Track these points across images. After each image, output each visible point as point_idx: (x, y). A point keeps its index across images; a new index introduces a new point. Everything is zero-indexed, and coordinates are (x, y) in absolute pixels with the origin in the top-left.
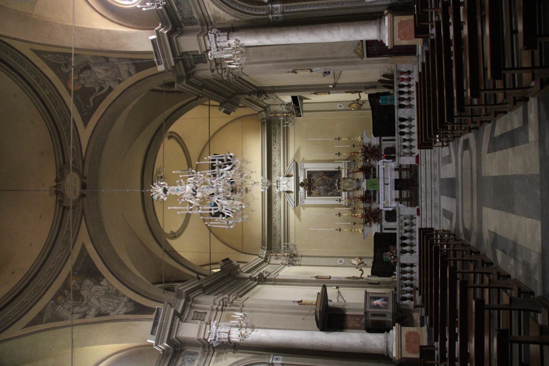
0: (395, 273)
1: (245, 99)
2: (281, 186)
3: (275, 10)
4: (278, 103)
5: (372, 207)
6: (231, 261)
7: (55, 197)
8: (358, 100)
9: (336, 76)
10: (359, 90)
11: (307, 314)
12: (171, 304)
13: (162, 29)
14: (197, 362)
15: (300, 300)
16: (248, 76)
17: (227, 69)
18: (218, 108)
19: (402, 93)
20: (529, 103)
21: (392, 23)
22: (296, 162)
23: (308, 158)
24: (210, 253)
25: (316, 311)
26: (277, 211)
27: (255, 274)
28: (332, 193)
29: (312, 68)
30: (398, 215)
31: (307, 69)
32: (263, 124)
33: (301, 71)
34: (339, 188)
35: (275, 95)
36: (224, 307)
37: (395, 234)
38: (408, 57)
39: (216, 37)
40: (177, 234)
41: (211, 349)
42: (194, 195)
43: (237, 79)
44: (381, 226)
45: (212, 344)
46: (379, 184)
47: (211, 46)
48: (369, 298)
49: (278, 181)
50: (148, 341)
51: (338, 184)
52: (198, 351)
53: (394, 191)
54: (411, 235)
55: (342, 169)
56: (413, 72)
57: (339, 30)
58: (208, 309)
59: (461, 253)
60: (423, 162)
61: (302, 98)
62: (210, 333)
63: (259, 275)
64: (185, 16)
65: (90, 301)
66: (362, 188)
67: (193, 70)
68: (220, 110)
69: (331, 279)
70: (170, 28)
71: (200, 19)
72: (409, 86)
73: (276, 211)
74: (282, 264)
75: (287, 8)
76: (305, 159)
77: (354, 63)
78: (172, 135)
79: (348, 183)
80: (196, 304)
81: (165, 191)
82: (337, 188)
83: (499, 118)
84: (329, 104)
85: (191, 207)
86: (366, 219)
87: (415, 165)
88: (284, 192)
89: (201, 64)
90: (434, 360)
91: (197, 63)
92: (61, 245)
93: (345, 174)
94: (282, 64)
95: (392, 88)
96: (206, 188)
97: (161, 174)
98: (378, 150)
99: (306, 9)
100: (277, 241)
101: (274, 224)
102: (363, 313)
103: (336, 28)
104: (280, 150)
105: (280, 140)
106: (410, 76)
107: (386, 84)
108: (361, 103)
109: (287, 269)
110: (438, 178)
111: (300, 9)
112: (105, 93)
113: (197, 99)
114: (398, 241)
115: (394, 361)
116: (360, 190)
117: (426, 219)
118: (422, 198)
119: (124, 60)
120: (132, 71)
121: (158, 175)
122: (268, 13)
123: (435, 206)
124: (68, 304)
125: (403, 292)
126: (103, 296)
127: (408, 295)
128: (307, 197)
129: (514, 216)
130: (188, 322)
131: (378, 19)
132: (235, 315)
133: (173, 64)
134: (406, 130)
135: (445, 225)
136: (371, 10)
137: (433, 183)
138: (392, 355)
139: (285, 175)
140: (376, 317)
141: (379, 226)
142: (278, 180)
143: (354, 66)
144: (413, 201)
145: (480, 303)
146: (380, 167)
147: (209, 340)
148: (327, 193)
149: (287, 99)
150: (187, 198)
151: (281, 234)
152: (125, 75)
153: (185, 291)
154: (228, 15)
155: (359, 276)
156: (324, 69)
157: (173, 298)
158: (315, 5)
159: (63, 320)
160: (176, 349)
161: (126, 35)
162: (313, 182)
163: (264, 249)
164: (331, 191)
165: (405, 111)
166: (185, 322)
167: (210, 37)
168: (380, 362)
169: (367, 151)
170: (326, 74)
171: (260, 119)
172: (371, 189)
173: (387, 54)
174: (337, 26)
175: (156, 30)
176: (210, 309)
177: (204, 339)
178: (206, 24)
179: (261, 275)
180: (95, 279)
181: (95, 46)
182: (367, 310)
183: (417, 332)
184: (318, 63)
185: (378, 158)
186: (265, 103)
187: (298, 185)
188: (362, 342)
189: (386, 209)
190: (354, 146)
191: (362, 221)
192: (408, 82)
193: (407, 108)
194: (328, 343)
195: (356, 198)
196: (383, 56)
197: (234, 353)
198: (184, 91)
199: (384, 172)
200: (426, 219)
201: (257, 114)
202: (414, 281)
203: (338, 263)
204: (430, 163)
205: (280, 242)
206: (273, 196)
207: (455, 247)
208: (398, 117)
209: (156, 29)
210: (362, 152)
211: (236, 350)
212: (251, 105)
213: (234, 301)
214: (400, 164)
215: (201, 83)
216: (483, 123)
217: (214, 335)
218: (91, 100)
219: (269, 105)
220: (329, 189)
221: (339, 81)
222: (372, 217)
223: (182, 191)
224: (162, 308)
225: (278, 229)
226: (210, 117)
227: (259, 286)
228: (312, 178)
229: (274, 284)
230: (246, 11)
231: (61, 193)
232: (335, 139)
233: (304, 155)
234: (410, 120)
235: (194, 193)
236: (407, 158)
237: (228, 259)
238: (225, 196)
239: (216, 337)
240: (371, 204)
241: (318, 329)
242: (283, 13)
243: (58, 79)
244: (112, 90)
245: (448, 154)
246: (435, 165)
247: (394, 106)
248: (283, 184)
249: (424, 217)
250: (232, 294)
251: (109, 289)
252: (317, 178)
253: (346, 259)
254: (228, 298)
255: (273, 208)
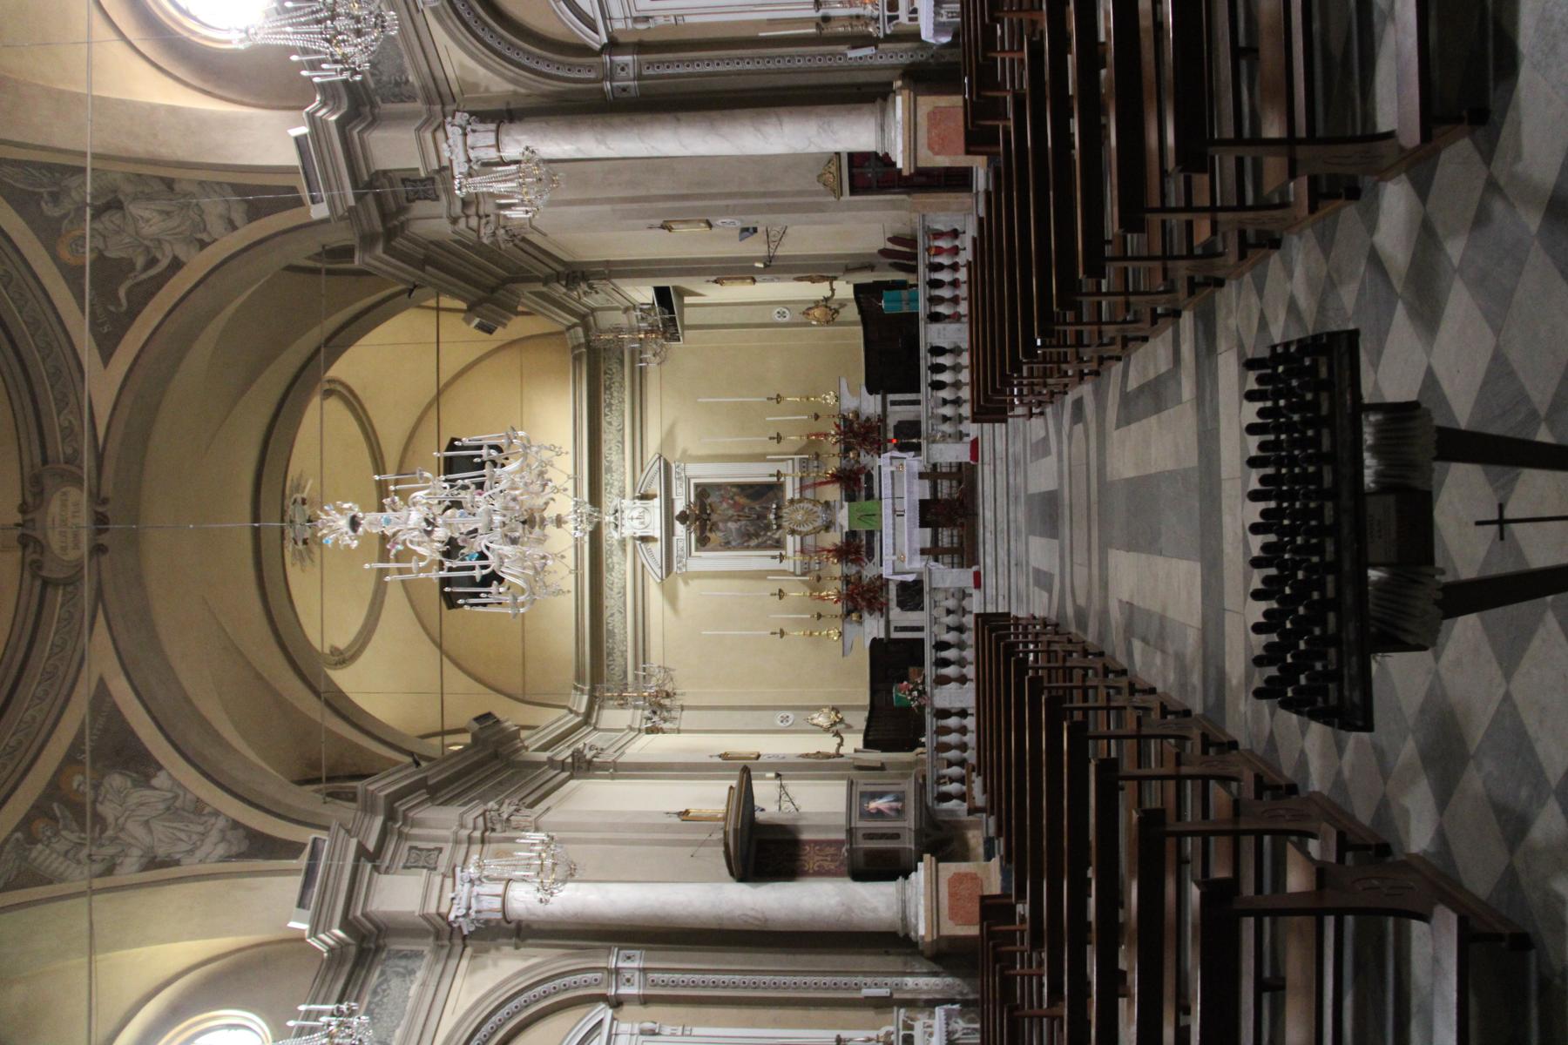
0: (923, 740)
1: (531, 293)
2: (627, 523)
3: (619, 69)
4: (617, 304)
5: (865, 573)
6: (498, 722)
7: (19, 554)
8: (826, 299)
9: (772, 239)
10: (830, 275)
11: (703, 844)
12: (348, 831)
13: (324, 111)
14: (420, 975)
15: (683, 810)
16: (545, 235)
17: (492, 218)
18: (462, 315)
19: (936, 284)
20: (1181, 320)
21: (912, 112)
22: (665, 460)
23: (695, 450)
24: (442, 694)
25: (725, 833)
26: (616, 590)
27: (564, 753)
28: (760, 540)
29: (711, 220)
30: (926, 588)
31: (700, 221)
32: (577, 359)
33: (684, 226)
34: (779, 527)
35: (613, 284)
36: (487, 834)
37: (921, 641)
38: (953, 195)
39: (465, 135)
40: (347, 655)
41: (458, 942)
42: (429, 533)
43: (517, 242)
44: (888, 623)
45: (460, 927)
46: (881, 515)
47: (453, 157)
48: (857, 798)
49: (616, 511)
50: (293, 924)
51: (776, 514)
52: (420, 948)
53: (917, 531)
54: (960, 638)
55: (785, 475)
56: (964, 232)
57: (781, 125)
58: (446, 840)
59: (1081, 672)
60: (987, 457)
61: (682, 293)
62: (453, 899)
63: (572, 755)
64: (385, 78)
65: (122, 829)
66: (837, 525)
67: (402, 218)
68: (468, 322)
69: (760, 760)
70: (344, 108)
71: (424, 87)
72: (954, 267)
73: (612, 590)
74: (631, 729)
75: (650, 64)
76: (689, 452)
77: (820, 208)
78: (333, 386)
79: (801, 512)
80: (412, 827)
81: (354, 523)
82: (775, 527)
83: (1135, 351)
84: (753, 307)
85: (421, 564)
86: (850, 603)
87: (967, 463)
88: (634, 539)
89: (428, 202)
90: (1014, 923)
91: (413, 201)
92: (39, 684)
93: (794, 490)
94: (635, 206)
95: (913, 270)
96: (460, 516)
97: (303, 492)
98: (879, 427)
99: (698, 69)
100: (618, 670)
101: (608, 623)
102: (842, 836)
103: (774, 120)
104: (623, 429)
105: (623, 401)
106: (957, 243)
107: (901, 261)
108: (837, 307)
109: (646, 739)
110: (1023, 495)
111: (682, 70)
112: (160, 274)
113: (411, 291)
114: (929, 655)
115: (921, 948)
116: (832, 530)
117: (997, 595)
118: (987, 546)
119: (217, 188)
120: (238, 217)
121: (295, 496)
122: (600, 77)
123: (1016, 565)
124: (63, 840)
125: (940, 780)
126: (160, 815)
127: (953, 788)
128: (694, 553)
129: (1160, 560)
130: (394, 874)
131: (879, 101)
132: (524, 838)
133: (351, 202)
134: (946, 377)
135: (1038, 605)
136: (862, 78)
137: (1012, 508)
138: (916, 932)
139: (637, 494)
140: (875, 841)
141: (882, 622)
142: (619, 507)
143: (816, 216)
144: (966, 553)
145: (1108, 768)
146: (883, 469)
147: (452, 917)
148: (747, 541)
149: (644, 293)
150: (411, 542)
151: (626, 651)
152: (216, 226)
153: (383, 794)
154: (498, 79)
155: (832, 750)
156: (742, 221)
157: (352, 815)
158: (722, 60)
159: (50, 882)
160: (365, 945)
161: (225, 122)
162: (712, 510)
163: (582, 691)
164: (757, 535)
165: (944, 329)
166: (387, 872)
167: (450, 135)
168: (887, 953)
169: (852, 431)
170: (746, 233)
171: (570, 346)
172: (862, 528)
173: (900, 187)
174: (778, 116)
175: (308, 113)
176: (451, 839)
177: (439, 915)
178: (439, 100)
179: (577, 755)
180: (137, 772)
181: (139, 148)
182: (853, 825)
183: (975, 874)
184: (727, 206)
185: (879, 449)
186: (583, 305)
187: (669, 518)
188: (843, 905)
189: (899, 578)
190: (817, 417)
191: (838, 608)
192: (953, 258)
193: (950, 323)
194: (757, 911)
195: (824, 550)
196: (893, 190)
197: (517, 948)
198: (371, 270)
199: (893, 484)
200: (997, 595)
201: (561, 333)
202: (969, 752)
203: (779, 722)
204: (1004, 459)
205: (625, 673)
206: (604, 550)
207: (1068, 658)
208: (926, 344)
209: (307, 110)
210: (837, 434)
211: (524, 939)
212: (545, 308)
213: (512, 818)
214: (932, 461)
215: (422, 251)
216: (1105, 363)
217: (464, 903)
218: (122, 293)
219: (593, 310)
220: (751, 529)
221: (780, 252)
222: (863, 598)
223: (397, 524)
224: (327, 838)
225: (618, 638)
226: (441, 340)
227: (573, 783)
228: (709, 501)
229: (613, 777)
230: (546, 70)
231: (37, 541)
232: (768, 399)
233: (686, 440)
234: (956, 351)
235: (429, 529)
236: (951, 445)
237: (488, 716)
238: (506, 536)
239: (469, 908)
240: (860, 565)
241: (731, 878)
242: (639, 77)
243: (30, 234)
244: (182, 267)
245: (1042, 434)
246: (1017, 463)
247: (917, 314)
248: (632, 519)
249: (991, 591)
250: (507, 801)
251: (176, 797)
252: (721, 502)
253: (796, 712)
254: (498, 810)
255: (605, 582)
